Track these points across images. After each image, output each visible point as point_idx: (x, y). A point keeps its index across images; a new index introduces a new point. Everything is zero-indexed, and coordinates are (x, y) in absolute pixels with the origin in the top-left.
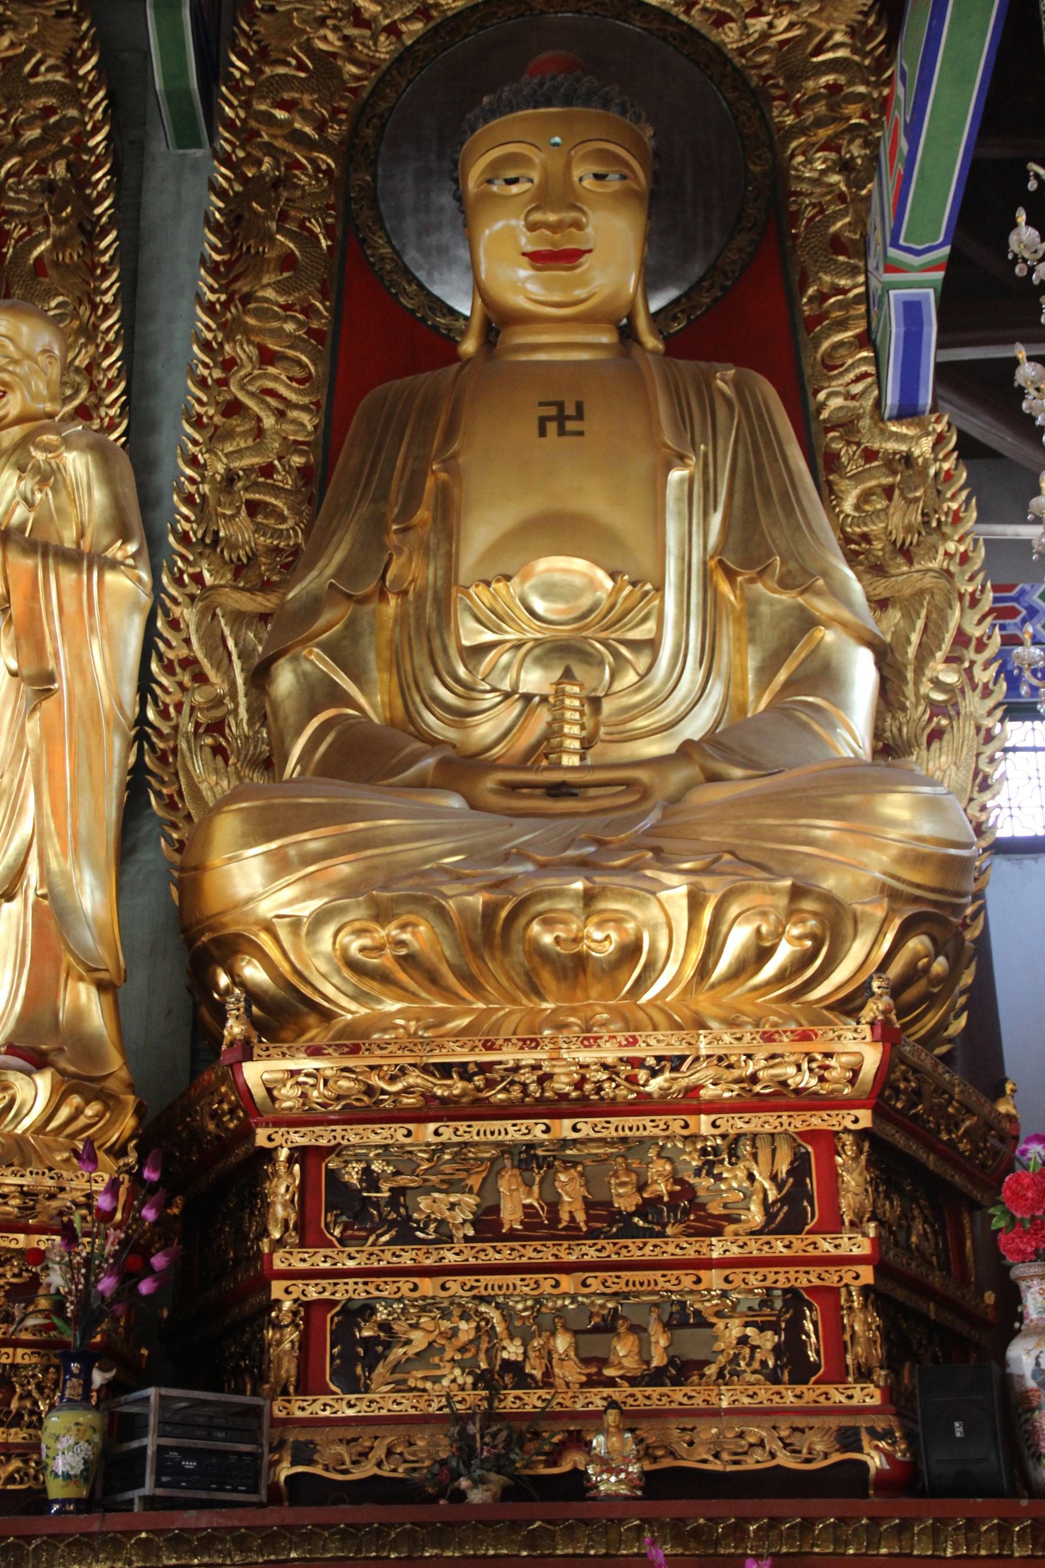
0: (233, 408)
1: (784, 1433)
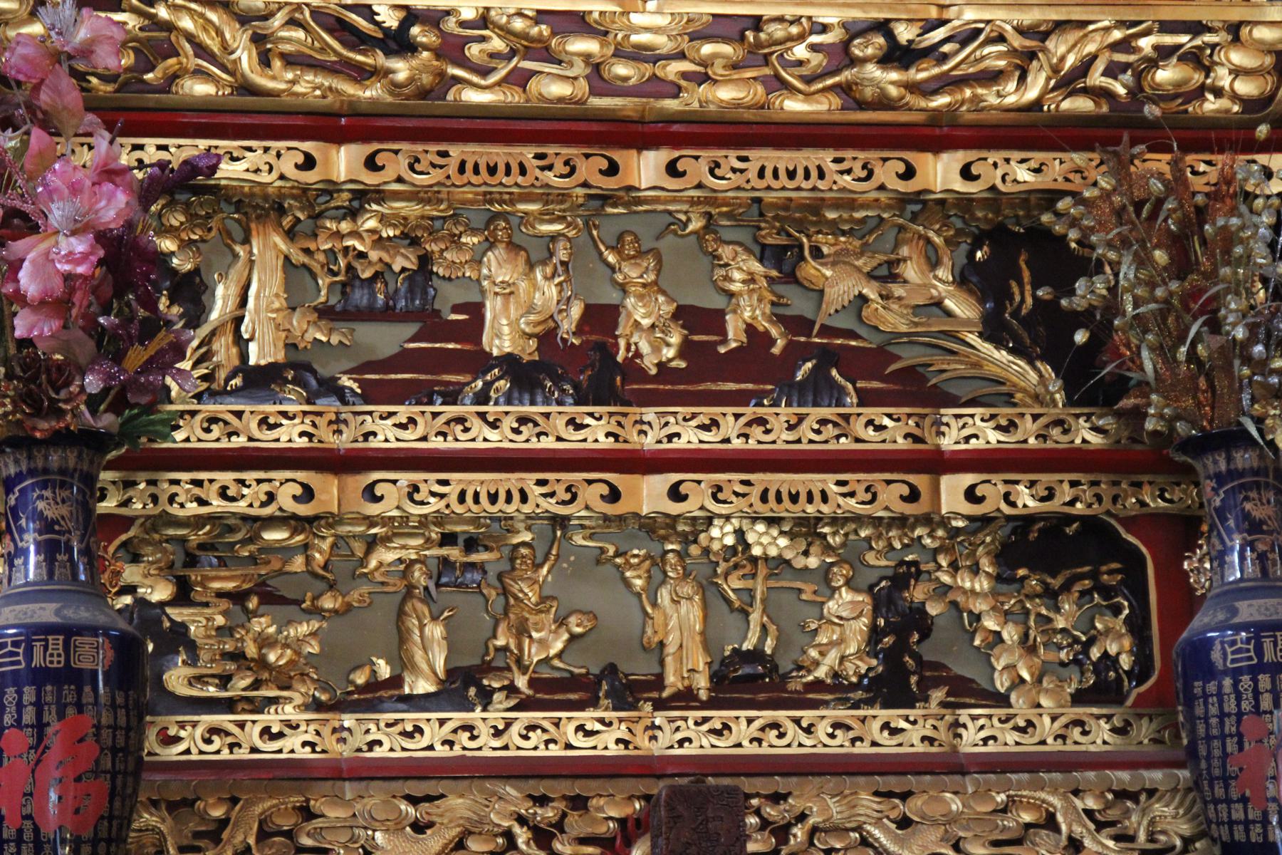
1: (1091, 803)
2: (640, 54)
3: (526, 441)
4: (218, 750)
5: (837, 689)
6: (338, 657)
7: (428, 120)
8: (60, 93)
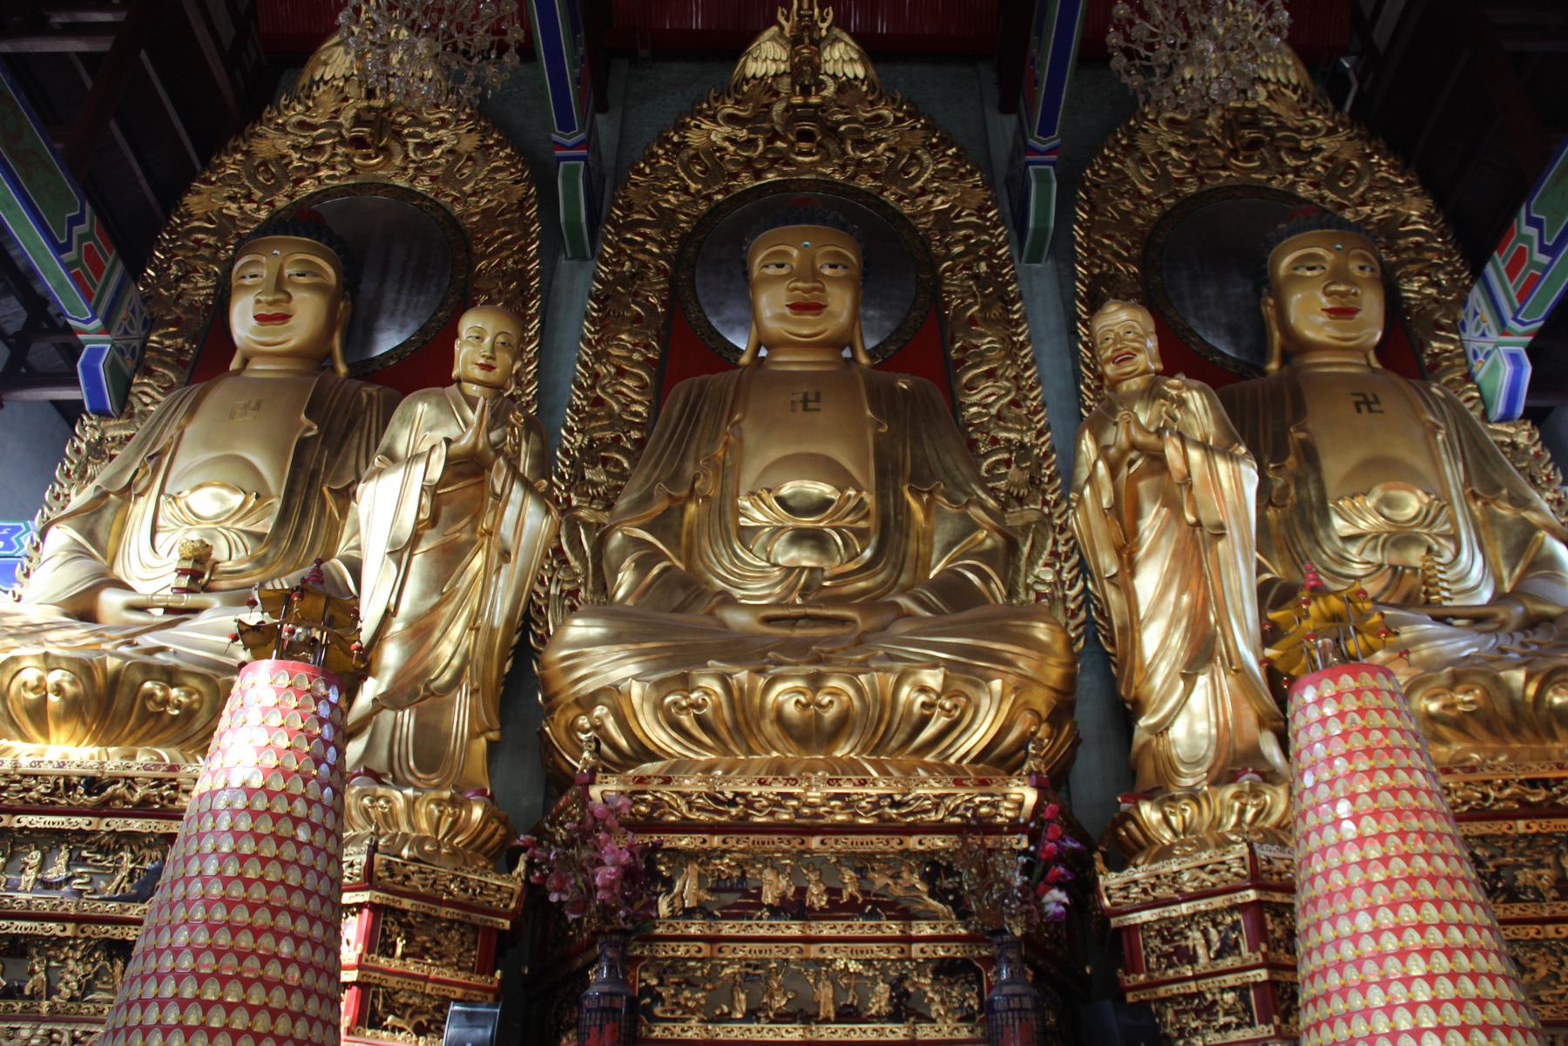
0: (598, 402)
2: (811, 805)
3: (771, 933)
5: (878, 1018)
6: (712, 1003)
7: (742, 827)
8: (612, 821)
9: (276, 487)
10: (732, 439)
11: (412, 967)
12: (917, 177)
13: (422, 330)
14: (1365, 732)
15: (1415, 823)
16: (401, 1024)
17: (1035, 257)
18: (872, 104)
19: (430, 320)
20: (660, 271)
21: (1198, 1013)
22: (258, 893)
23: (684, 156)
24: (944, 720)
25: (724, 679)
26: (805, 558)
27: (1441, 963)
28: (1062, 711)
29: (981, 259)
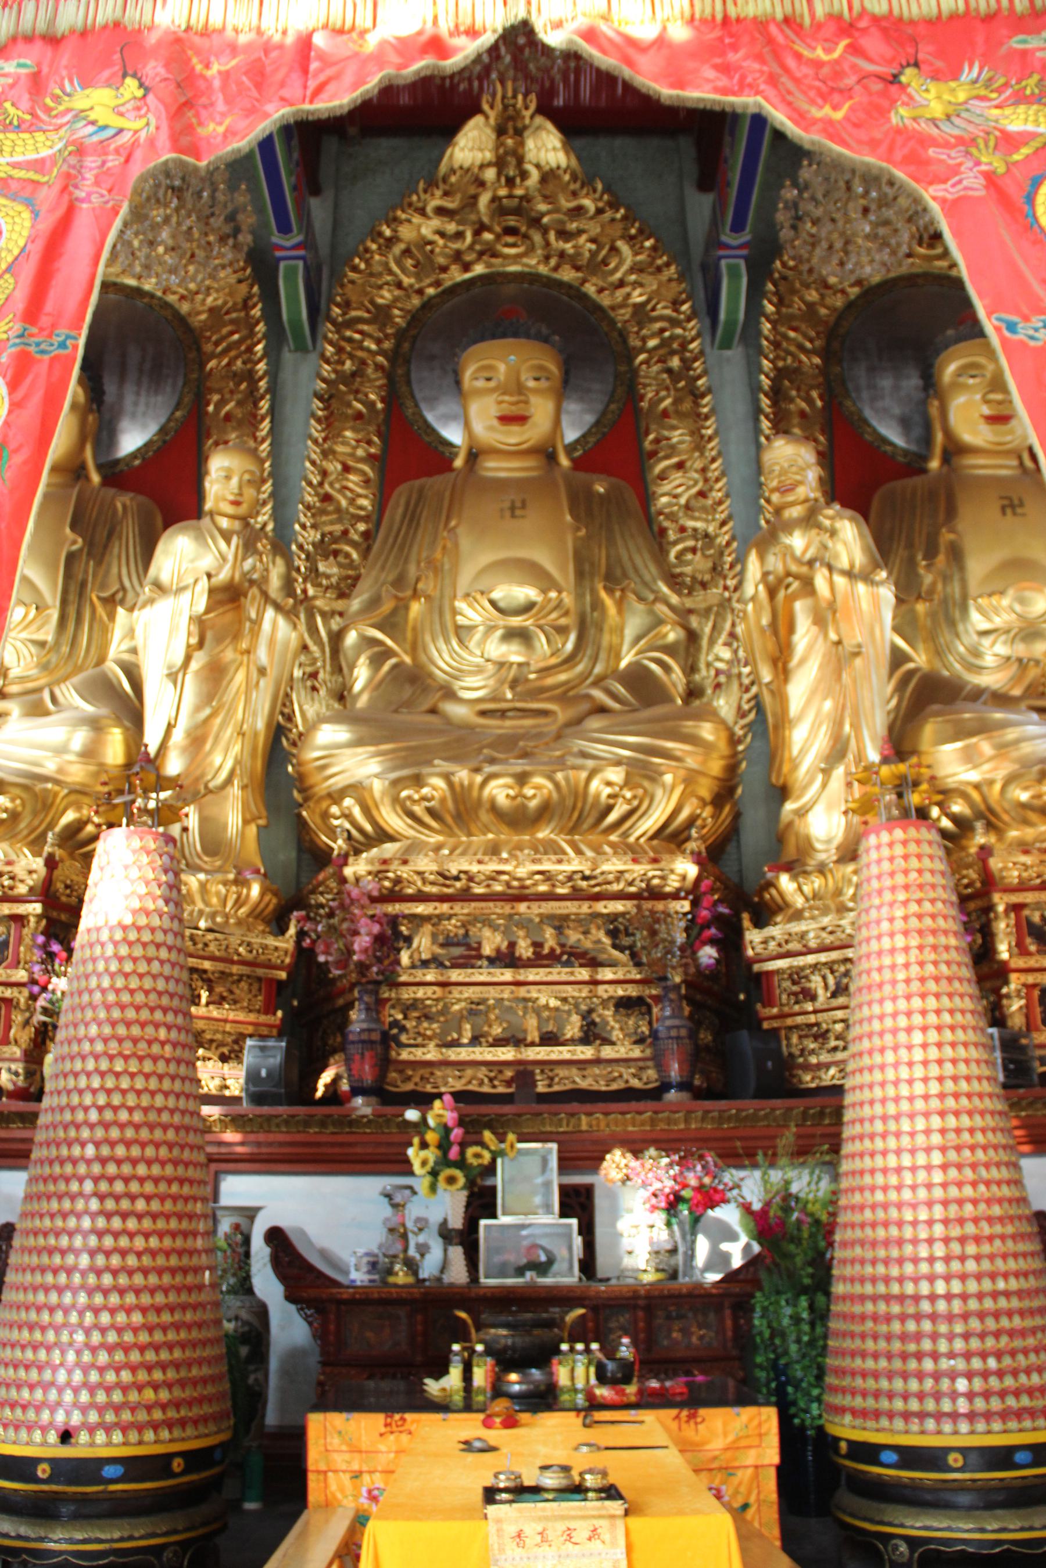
0: (327, 498)
2: (519, 879)
4: (411, 1058)
5: (572, 1042)
6: (445, 1032)
7: (465, 896)
9: (52, 598)
10: (449, 545)
11: (215, 1012)
12: (616, 269)
13: (163, 430)
14: (906, 872)
15: (930, 940)
16: (208, 1054)
17: (726, 345)
18: (575, 194)
19: (169, 420)
20: (378, 367)
21: (816, 1037)
22: (140, 998)
23: (398, 249)
24: (626, 808)
25: (447, 777)
26: (514, 654)
27: (933, 1036)
28: (724, 793)
29: (673, 353)
